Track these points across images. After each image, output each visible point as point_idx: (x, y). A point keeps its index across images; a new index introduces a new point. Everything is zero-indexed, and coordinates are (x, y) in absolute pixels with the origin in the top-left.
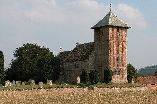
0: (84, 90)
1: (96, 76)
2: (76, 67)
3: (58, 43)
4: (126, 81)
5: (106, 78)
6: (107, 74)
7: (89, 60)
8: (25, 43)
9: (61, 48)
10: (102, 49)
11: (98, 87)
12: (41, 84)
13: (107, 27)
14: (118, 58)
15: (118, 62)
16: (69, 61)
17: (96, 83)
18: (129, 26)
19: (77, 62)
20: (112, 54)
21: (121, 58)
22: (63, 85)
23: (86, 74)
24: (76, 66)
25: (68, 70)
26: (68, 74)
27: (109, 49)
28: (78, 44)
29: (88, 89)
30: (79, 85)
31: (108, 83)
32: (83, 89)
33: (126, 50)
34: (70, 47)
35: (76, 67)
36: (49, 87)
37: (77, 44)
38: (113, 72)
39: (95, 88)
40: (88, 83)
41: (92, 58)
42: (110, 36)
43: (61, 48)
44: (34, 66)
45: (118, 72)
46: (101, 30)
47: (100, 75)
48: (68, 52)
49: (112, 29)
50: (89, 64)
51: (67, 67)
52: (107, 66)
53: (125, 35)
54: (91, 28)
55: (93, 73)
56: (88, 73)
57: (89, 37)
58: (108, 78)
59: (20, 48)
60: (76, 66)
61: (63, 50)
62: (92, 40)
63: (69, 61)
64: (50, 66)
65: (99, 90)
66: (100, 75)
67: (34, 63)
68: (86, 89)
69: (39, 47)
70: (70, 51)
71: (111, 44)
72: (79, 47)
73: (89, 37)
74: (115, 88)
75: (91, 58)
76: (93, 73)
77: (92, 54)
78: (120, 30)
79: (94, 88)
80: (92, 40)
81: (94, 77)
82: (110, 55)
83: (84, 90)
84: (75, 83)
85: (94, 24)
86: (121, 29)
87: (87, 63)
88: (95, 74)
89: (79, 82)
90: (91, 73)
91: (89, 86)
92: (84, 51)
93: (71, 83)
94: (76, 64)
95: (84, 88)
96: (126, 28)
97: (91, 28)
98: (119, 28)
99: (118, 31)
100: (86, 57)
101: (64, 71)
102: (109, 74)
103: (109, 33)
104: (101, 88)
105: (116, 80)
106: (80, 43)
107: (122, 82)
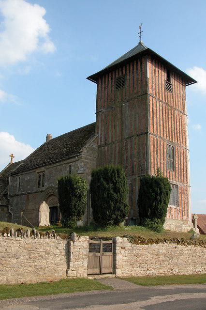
0: (68, 253)
1: (117, 190)
2: (39, 184)
6: (154, 191)
7: (81, 158)
9: (12, 156)
10: (122, 123)
11: (134, 240)
19: (43, 169)
21: (177, 156)
23: (74, 189)
24: (39, 181)
25: (18, 195)
26: (17, 204)
27: (149, 117)
28: (51, 139)
29: (90, 244)
31: (155, 225)
32: (63, 244)
33: (187, 137)
35: (39, 184)
37: (47, 137)
39: (119, 239)
40: (80, 223)
41: (91, 152)
42: (150, 85)
43: (12, 156)
47: (128, 194)
49: (154, 67)
51: (18, 186)
53: (182, 96)
55: (108, 179)
58: (156, 208)
66: (128, 194)
68: (81, 243)
71: (155, 108)
73: (80, 110)
74: (188, 244)
75: (88, 152)
76: (108, 179)
79: (115, 242)
81: (110, 197)
82: (151, 138)
83: (68, 253)
86: (175, 79)
87: (73, 168)
88: (115, 184)
89: (44, 219)
90: (99, 179)
91: (93, 234)
94: (40, 176)
95: (70, 238)
101: (10, 197)
102: (161, 192)
103: (149, 76)
104: (143, 243)
107: (181, 227)
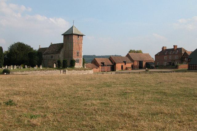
3: (37, 42)
4: (81, 66)
5: (72, 64)
8: (16, 42)
12: (31, 68)
13: (72, 34)
14: (78, 53)
15: (78, 55)
16: (47, 54)
17: (66, 68)
18: (81, 33)
20: (75, 51)
22: (48, 68)
30: (55, 68)
34: (46, 45)
36: (41, 70)
38: (177, 69)
44: (21, 56)
45: (78, 61)
46: (68, 36)
48: (45, 49)
50: (61, 56)
52: (72, 57)
54: (62, 35)
56: (62, 62)
57: (61, 40)
59: (12, 45)
60: (52, 57)
61: (41, 47)
62: (62, 42)
63: (47, 54)
64: (37, 57)
65: (69, 72)
67: (22, 55)
69: (24, 45)
70: (47, 48)
72: (52, 46)
73: (61, 40)
77: (62, 50)
78: (79, 37)
80: (62, 42)
84: (53, 67)
85: (64, 31)
89: (55, 66)
92: (56, 48)
93: (50, 67)
96: (82, 36)
97: (62, 35)
98: (78, 35)
99: (78, 37)
100: (59, 52)
103: (74, 38)
105: (77, 66)
106: (53, 43)
